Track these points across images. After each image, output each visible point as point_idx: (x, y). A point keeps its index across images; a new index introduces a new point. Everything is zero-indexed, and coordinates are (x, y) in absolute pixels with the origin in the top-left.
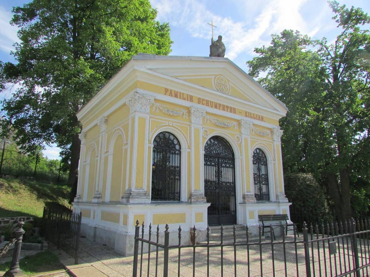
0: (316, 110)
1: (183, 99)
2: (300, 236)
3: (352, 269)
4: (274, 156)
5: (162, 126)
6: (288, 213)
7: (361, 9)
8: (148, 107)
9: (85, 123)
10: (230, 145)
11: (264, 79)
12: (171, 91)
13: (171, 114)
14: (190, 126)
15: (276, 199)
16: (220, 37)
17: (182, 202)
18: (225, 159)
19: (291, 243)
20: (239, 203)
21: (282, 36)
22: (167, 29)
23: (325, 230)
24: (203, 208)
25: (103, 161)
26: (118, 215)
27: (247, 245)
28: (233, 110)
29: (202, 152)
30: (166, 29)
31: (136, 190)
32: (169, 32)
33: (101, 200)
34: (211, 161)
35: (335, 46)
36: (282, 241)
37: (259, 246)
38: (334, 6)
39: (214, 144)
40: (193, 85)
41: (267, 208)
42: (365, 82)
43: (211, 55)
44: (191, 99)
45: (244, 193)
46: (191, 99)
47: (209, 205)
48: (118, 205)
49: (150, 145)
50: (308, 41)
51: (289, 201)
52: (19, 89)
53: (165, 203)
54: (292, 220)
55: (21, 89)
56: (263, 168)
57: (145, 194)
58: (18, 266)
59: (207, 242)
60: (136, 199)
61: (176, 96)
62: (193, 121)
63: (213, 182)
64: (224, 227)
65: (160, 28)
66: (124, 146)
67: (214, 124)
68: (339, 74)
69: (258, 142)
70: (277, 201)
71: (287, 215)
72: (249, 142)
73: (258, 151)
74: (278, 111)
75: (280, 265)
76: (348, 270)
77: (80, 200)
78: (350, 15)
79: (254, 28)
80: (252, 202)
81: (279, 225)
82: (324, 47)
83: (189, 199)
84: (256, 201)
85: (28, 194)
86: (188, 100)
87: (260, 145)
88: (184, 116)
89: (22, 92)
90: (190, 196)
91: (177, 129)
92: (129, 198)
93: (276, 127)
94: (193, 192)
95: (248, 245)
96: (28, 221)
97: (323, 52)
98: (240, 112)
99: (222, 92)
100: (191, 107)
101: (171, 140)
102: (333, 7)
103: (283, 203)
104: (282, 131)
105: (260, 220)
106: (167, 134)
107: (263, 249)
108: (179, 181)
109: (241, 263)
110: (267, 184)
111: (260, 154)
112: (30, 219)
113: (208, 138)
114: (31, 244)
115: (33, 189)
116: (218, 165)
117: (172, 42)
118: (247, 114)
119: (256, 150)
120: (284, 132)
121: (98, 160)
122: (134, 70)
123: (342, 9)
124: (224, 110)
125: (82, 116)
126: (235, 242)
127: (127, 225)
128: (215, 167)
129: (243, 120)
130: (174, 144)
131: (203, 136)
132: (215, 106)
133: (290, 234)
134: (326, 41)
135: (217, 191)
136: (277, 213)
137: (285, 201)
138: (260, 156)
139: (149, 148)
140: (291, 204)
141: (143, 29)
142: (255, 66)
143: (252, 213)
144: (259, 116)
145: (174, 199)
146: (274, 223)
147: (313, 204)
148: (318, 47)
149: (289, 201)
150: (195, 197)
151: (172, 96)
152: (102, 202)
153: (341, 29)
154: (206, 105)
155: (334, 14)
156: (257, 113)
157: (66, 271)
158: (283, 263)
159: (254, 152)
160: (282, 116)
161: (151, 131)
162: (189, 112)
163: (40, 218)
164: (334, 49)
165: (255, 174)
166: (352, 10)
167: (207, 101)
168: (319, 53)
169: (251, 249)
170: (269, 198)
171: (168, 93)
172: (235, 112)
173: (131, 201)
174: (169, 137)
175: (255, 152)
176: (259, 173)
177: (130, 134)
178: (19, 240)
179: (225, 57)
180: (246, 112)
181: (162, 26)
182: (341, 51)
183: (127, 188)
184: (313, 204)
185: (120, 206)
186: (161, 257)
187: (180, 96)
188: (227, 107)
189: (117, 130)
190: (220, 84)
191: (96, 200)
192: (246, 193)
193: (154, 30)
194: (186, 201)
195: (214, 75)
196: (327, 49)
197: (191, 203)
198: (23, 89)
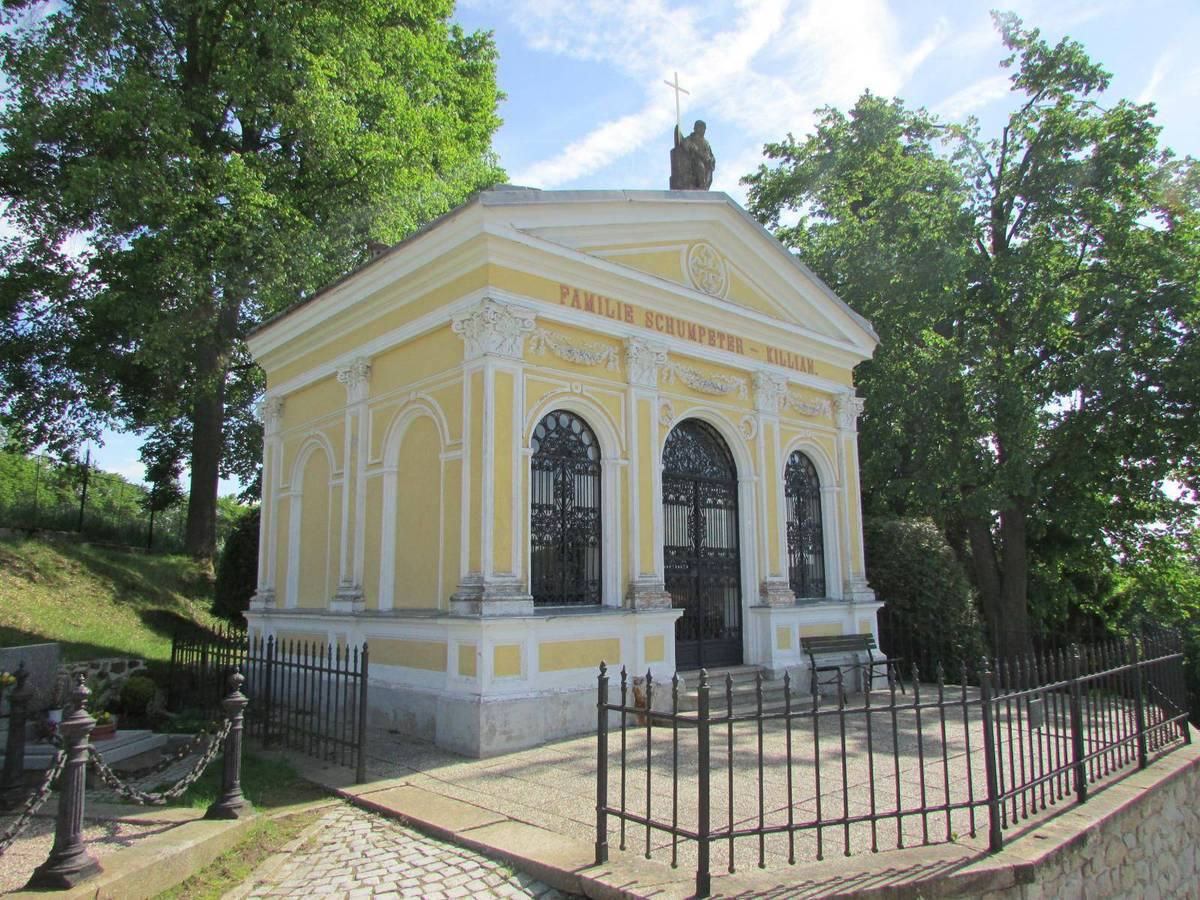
0: (943, 329)
1: (608, 316)
2: (907, 692)
3: (1070, 760)
5: (556, 396)
7: (1082, 46)
8: (520, 341)
9: (274, 369)
10: (726, 444)
11: (792, 230)
12: (576, 291)
13: (578, 361)
14: (625, 391)
16: (700, 127)
17: (607, 607)
18: (713, 483)
19: (956, 704)
22: (486, 53)
23: (1022, 674)
24: (662, 623)
25: (361, 491)
26: (444, 648)
27: (787, 720)
28: (735, 344)
29: (658, 467)
30: (484, 52)
32: (494, 61)
33: (361, 606)
34: (677, 490)
35: (1002, 143)
36: (863, 707)
37: (812, 719)
38: (1008, 29)
39: (683, 440)
40: (635, 276)
41: (824, 618)
42: (1079, 253)
43: (675, 183)
44: (627, 313)
46: (627, 313)
47: (680, 613)
48: (440, 621)
49: (527, 450)
50: (927, 127)
52: (9, 241)
53: (573, 611)
54: (883, 649)
55: (16, 239)
57: (518, 589)
58: (238, 791)
60: (498, 603)
61: (589, 307)
62: (633, 380)
63: (683, 548)
64: (707, 673)
65: (464, 48)
66: (445, 451)
67: (686, 385)
68: (1009, 228)
69: (798, 433)
70: (847, 597)
71: (871, 635)
72: (777, 438)
73: (797, 459)
74: (849, 341)
75: (884, 763)
76: (1028, 780)
77: (273, 606)
78: (1051, 63)
79: (734, 29)
80: (785, 603)
81: (852, 662)
82: (970, 146)
83: (627, 598)
84: (794, 598)
85: (87, 589)
86: (620, 318)
87: (801, 442)
88: (611, 363)
89: (15, 252)
90: (631, 592)
91: (594, 402)
92: (479, 599)
93: (846, 390)
94: (637, 579)
95: (789, 718)
96: (133, 670)
97: (966, 160)
98: (752, 350)
99: (707, 294)
100: (628, 339)
101: (575, 435)
102: (1006, 30)
103: (862, 603)
104: (861, 401)
105: (806, 652)
106: (564, 419)
107: (820, 734)
108: (597, 551)
109: (800, 762)
110: (820, 553)
112: (136, 664)
114: (187, 736)
115: (97, 569)
116: (695, 500)
117: (500, 97)
118: (773, 356)
119: (557, 420)
120: (865, 403)
121: (341, 487)
122: (484, 233)
123: (1030, 41)
124: (713, 345)
125: (268, 349)
126: (760, 710)
127: (474, 675)
129: (762, 372)
130: (581, 444)
133: (880, 686)
134: (978, 129)
135: (694, 573)
136: (847, 631)
137: (867, 599)
139: (525, 457)
140: (882, 605)
141: (419, 57)
142: (767, 195)
143: (784, 633)
144: (803, 358)
145: (578, 598)
146: (838, 658)
147: (938, 604)
148: (956, 143)
150: (642, 594)
151: (579, 307)
152: (366, 611)
153: (1023, 97)
154: (668, 332)
155: (1006, 52)
156: (799, 352)
157: (348, 802)
158: (891, 760)
159: (543, 423)
160: (860, 356)
162: (624, 353)
164: (999, 151)
165: (790, 524)
166: (1061, 46)
167: (670, 320)
168: (957, 163)
169: (797, 728)
170: (824, 588)
171: (569, 299)
172: (740, 351)
173: (486, 609)
174: (570, 426)
177: (467, 416)
178: (235, 723)
179: (714, 187)
180: (769, 350)
181: (469, 39)
182: (1019, 158)
183: (465, 571)
184: (938, 604)
185: (450, 622)
187: (600, 304)
188: (721, 336)
189: (414, 402)
190: (702, 268)
191: (347, 607)
192: (769, 579)
193: (449, 57)
194: (620, 605)
195: (684, 242)
196: (979, 150)
197: (633, 609)
198: (19, 239)
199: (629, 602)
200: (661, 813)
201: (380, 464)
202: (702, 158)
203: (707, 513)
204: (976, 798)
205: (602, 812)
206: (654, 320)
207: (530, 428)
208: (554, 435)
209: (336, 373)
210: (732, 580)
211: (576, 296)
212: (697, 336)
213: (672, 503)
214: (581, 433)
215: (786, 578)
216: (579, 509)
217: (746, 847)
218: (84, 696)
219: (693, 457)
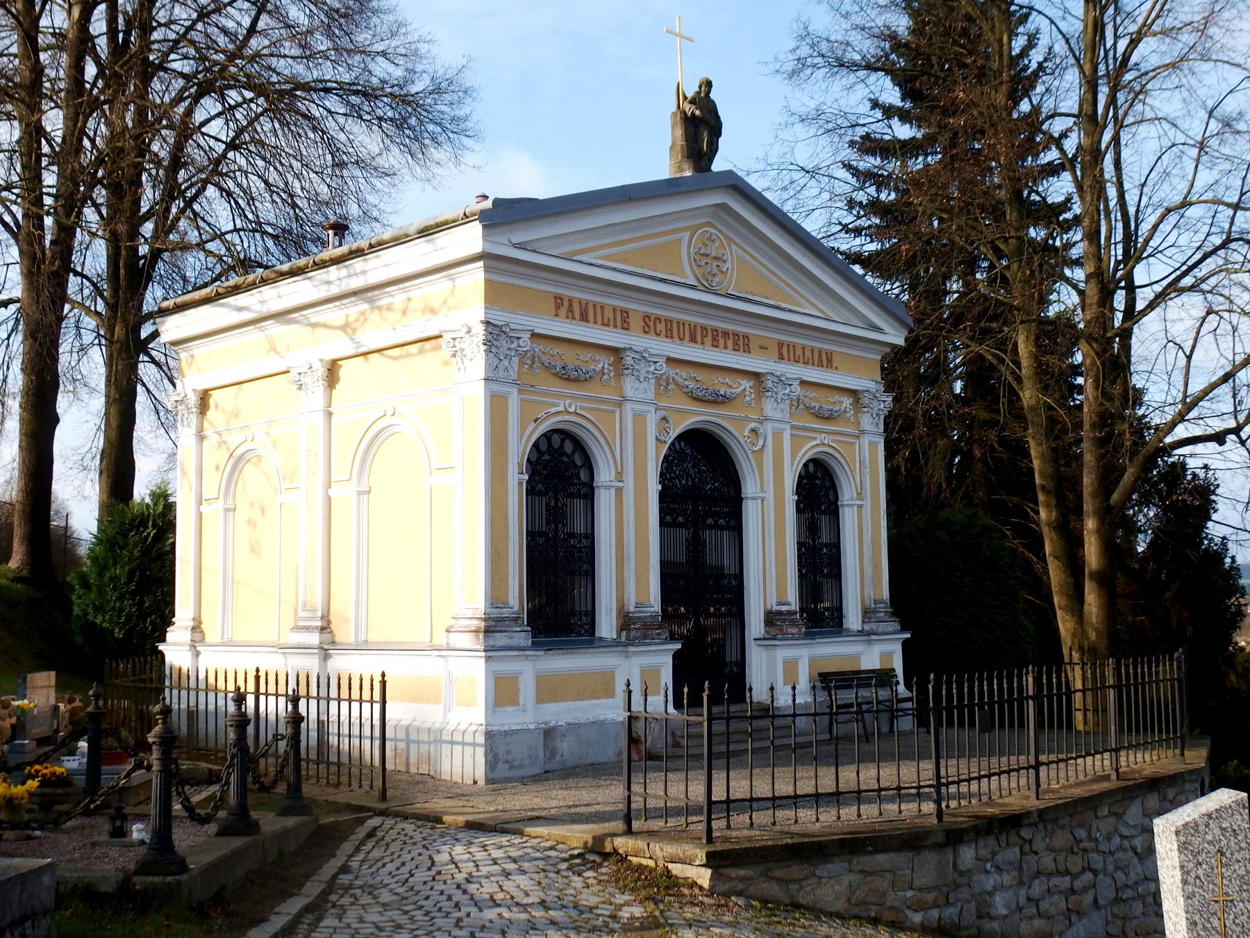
4: (861, 481)
6: (898, 665)
21: (1054, 148)
31: (494, 610)
56: (824, 521)
57: (516, 619)
69: (814, 439)
93: (871, 386)
131: (657, 439)
132: (582, 315)
137: (890, 629)
138: (562, 462)
139: (520, 483)
149: (903, 630)
163: (1229, 641)
167: (669, 321)
171: (563, 311)
172: (747, 350)
174: (562, 446)
175: (544, 447)
176: (814, 541)
208: (546, 457)
211: (571, 305)
212: (699, 338)
214: (573, 454)
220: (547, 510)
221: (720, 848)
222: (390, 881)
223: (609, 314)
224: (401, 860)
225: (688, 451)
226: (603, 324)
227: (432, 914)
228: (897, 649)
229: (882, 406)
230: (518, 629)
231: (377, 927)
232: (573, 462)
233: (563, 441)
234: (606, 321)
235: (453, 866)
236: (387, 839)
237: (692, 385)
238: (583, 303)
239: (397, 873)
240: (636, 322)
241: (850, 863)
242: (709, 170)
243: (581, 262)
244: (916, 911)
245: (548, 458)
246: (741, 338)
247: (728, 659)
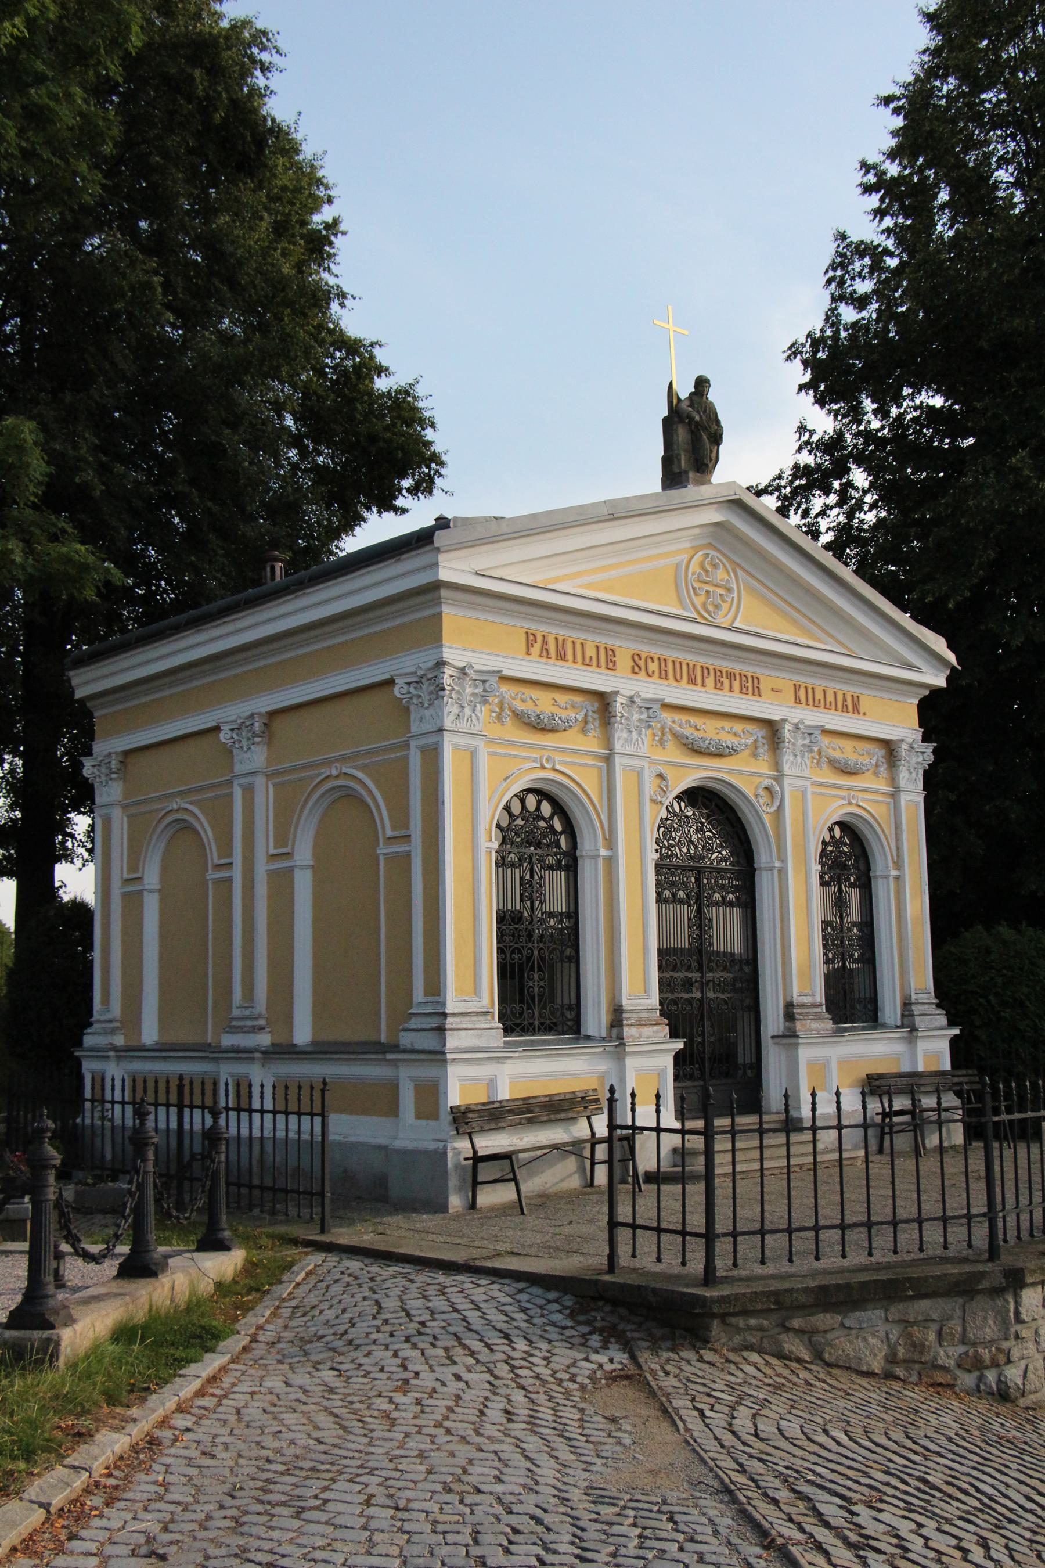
4: (898, 848)
15: (903, 1015)
16: (702, 384)
17: (588, 1038)
20: (773, 1037)
34: (673, 884)
39: (683, 820)
45: (789, 999)
51: (951, 1024)
59: (680, 1169)
84: (830, 1025)
101: (544, 819)
108: (573, 966)
111: (845, 844)
113: (516, 788)
119: (523, 801)
120: (935, 752)
128: (689, 905)
137: (937, 1024)
149: (951, 1024)
159: (507, 808)
161: (312, 778)
165: (826, 924)
167: (662, 661)
171: (536, 649)
172: (757, 692)
174: (538, 808)
186: (696, 1217)
192: (797, 999)
194: (604, 1034)
199: (615, 1031)
200: (671, 1220)
201: (288, 855)
202: (705, 429)
203: (713, 913)
204: (974, 1211)
205: (613, 1224)
206: (642, 663)
207: (493, 818)
208: (519, 822)
209: (217, 729)
210: (748, 1001)
211: (545, 642)
212: (699, 680)
213: (666, 901)
214: (551, 817)
215: (820, 997)
216: (551, 915)
217: (748, 1246)
218: (47, 1130)
219: (694, 838)
220: (521, 885)
221: (35, 1332)
222: (326, 1332)
223: (590, 652)
224: (342, 1306)
225: (690, 814)
226: (825, 708)
227: (372, 1375)
228: (944, 1046)
229: (920, 759)
230: (488, 1026)
231: (305, 1392)
232: (552, 828)
233: (539, 803)
234: (587, 661)
235: (403, 1314)
236: (329, 1279)
237: (688, 731)
238: (560, 639)
239: (337, 1321)
240: (624, 661)
241: (886, 1310)
242: (709, 482)
243: (501, 579)
244: (969, 1371)
245: (522, 823)
246: (750, 679)
247: (740, 1061)
